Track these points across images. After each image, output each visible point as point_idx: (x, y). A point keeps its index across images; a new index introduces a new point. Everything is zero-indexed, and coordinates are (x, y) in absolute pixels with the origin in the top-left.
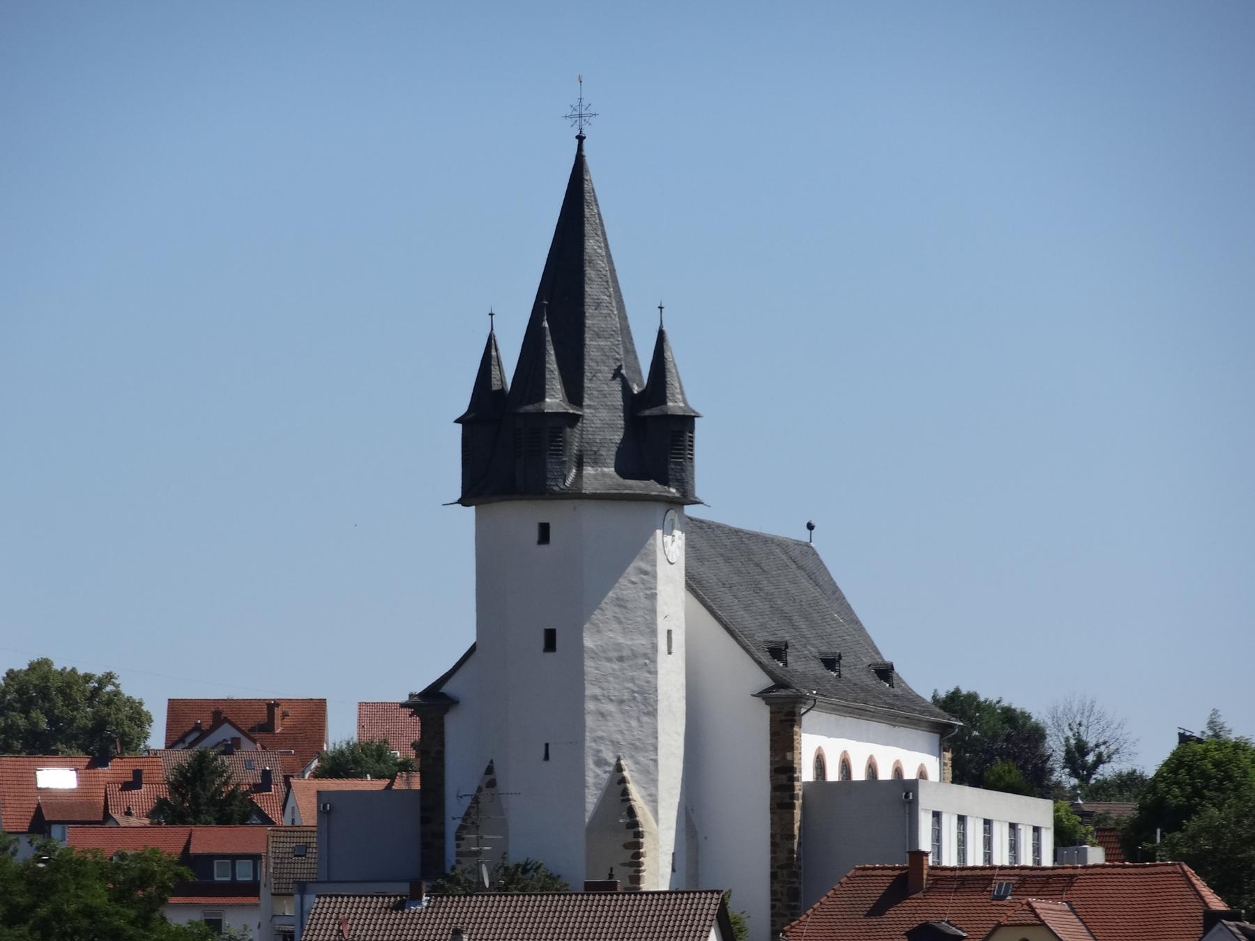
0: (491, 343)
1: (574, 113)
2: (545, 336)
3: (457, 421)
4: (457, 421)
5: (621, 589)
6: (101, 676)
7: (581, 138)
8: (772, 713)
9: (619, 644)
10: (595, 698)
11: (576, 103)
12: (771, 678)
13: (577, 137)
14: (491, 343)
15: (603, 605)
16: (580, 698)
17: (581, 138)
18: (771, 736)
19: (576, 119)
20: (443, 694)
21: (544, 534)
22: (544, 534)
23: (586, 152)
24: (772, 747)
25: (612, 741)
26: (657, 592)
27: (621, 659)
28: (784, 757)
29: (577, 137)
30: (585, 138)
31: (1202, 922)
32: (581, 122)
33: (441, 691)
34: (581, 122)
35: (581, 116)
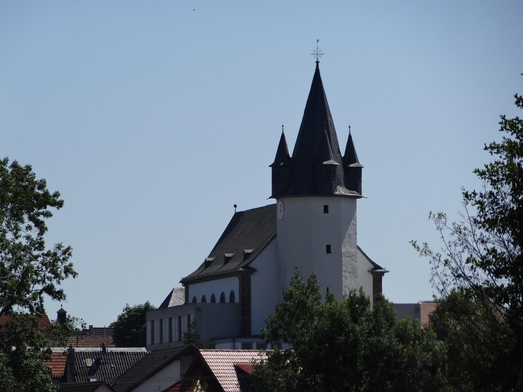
0: (283, 137)
1: (315, 53)
2: (326, 137)
3: (270, 166)
4: (270, 166)
5: (350, 231)
6: (481, 269)
7: (317, 62)
8: (373, 278)
9: (349, 251)
10: (345, 272)
11: (316, 50)
12: (373, 265)
13: (316, 62)
14: (283, 137)
15: (346, 237)
16: (341, 271)
17: (317, 62)
18: (373, 286)
19: (315, 55)
20: (249, 267)
21: (326, 209)
22: (326, 209)
23: (320, 67)
24: (373, 291)
25: (348, 287)
26: (357, 232)
27: (350, 257)
28: (379, 295)
29: (316, 62)
30: (319, 62)
31: (65, 360)
32: (317, 56)
33: (249, 266)
34: (317, 56)
35: (317, 54)
